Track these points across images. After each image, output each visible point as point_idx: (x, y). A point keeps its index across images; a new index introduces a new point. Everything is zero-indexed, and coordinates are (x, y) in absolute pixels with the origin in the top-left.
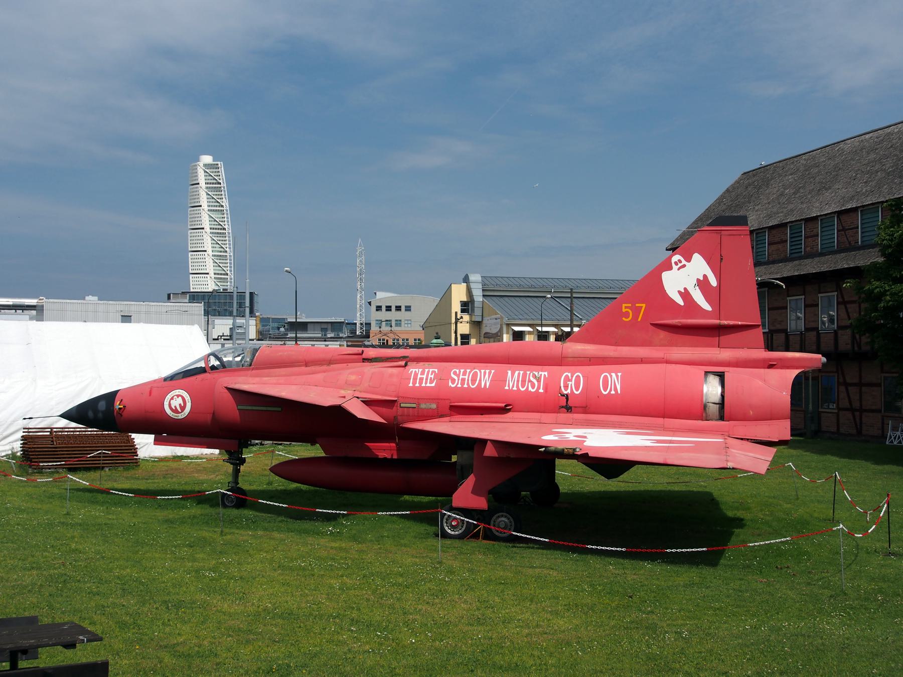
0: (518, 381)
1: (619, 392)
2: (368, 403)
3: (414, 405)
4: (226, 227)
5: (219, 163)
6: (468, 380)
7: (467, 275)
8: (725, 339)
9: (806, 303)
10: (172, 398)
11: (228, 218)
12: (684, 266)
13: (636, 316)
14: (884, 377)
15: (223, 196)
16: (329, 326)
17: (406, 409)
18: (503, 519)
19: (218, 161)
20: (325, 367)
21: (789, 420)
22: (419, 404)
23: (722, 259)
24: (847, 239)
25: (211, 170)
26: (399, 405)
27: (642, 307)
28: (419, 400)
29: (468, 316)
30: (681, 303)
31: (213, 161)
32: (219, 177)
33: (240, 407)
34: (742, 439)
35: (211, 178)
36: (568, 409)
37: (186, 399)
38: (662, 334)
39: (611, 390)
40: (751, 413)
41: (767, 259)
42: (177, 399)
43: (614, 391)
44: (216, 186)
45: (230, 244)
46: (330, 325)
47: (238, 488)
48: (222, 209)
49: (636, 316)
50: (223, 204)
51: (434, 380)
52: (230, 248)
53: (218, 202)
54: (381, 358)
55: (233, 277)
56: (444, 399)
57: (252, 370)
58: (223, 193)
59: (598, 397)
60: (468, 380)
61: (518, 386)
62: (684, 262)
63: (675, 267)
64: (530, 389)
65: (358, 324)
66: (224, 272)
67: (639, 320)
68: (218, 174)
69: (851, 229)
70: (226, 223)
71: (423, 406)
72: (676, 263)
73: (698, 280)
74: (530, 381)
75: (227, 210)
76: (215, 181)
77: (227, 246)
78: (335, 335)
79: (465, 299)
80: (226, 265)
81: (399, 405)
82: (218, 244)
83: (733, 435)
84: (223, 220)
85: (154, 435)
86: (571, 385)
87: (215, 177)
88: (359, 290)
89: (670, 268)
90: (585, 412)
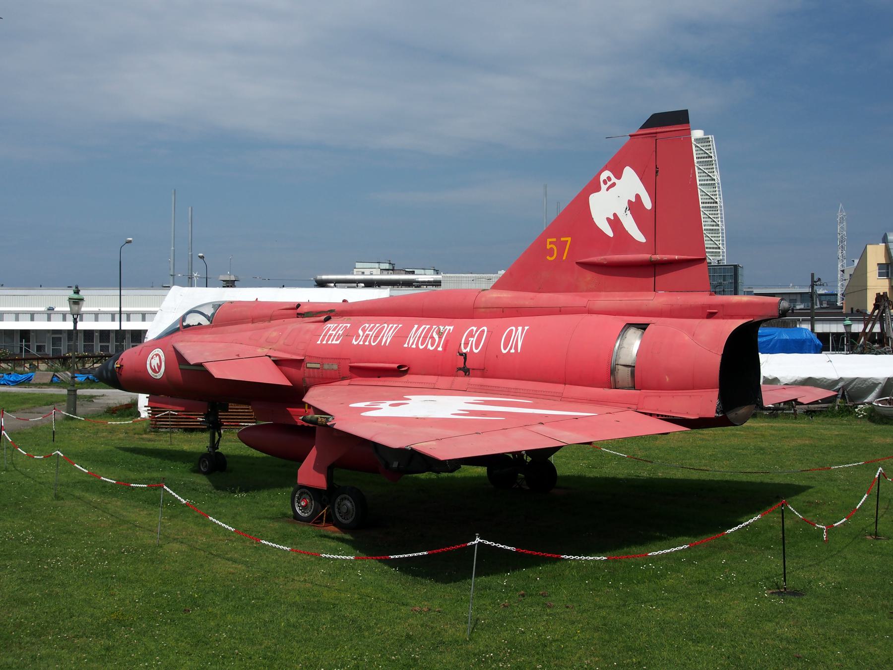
0: (419, 337)
1: (519, 351)
2: (278, 362)
3: (318, 366)
4: (717, 200)
5: (710, 136)
6: (372, 336)
7: (886, 234)
8: (664, 279)
10: (152, 358)
11: (719, 191)
12: (614, 185)
13: (560, 254)
15: (714, 170)
16: (799, 297)
17: (311, 369)
18: (349, 504)
19: (708, 135)
21: (718, 389)
22: (322, 365)
23: (657, 172)
25: (703, 144)
26: (305, 366)
27: (568, 241)
28: (322, 359)
29: (887, 280)
30: (609, 232)
31: (704, 135)
32: (710, 151)
33: (182, 367)
34: (651, 415)
35: (702, 152)
36: (466, 371)
37: (162, 358)
38: (589, 276)
39: (511, 349)
40: (668, 379)
43: (514, 349)
44: (708, 159)
45: (722, 218)
46: (799, 296)
47: (218, 452)
48: (714, 182)
49: (560, 254)
50: (715, 178)
51: (341, 336)
52: (722, 221)
53: (709, 176)
54: (312, 312)
55: (725, 250)
56: (345, 359)
57: (212, 327)
58: (714, 166)
59: (497, 356)
60: (372, 336)
61: (417, 344)
62: (614, 180)
63: (604, 187)
64: (429, 347)
65: (839, 295)
66: (716, 246)
67: (564, 258)
68: (709, 147)
70: (717, 196)
71: (326, 367)
72: (605, 182)
73: (630, 202)
74: (432, 337)
75: (718, 184)
76: (706, 155)
77: (719, 219)
78: (805, 306)
79: (883, 261)
80: (718, 239)
81: (305, 366)
82: (710, 218)
83: (642, 409)
84: (715, 193)
86: (473, 341)
87: (706, 151)
88: (841, 258)
89: (598, 189)
90: (483, 376)
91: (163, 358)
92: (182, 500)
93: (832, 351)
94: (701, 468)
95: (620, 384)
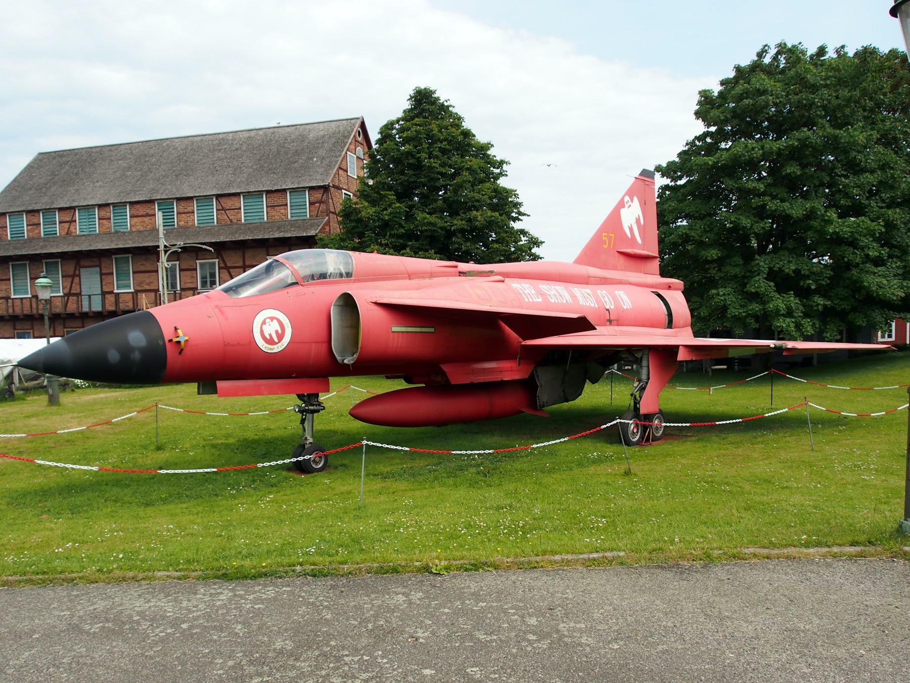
9: (181, 268)
10: (264, 323)
13: (610, 244)
14: (67, 331)
20: (427, 281)
24: (228, 217)
37: (284, 323)
38: (622, 260)
41: (129, 229)
42: (271, 323)
54: (474, 271)
62: (630, 203)
63: (627, 206)
69: (233, 209)
85: (197, 384)
89: (624, 206)
92: (93, 468)
94: (186, 211)
95: (118, 314)
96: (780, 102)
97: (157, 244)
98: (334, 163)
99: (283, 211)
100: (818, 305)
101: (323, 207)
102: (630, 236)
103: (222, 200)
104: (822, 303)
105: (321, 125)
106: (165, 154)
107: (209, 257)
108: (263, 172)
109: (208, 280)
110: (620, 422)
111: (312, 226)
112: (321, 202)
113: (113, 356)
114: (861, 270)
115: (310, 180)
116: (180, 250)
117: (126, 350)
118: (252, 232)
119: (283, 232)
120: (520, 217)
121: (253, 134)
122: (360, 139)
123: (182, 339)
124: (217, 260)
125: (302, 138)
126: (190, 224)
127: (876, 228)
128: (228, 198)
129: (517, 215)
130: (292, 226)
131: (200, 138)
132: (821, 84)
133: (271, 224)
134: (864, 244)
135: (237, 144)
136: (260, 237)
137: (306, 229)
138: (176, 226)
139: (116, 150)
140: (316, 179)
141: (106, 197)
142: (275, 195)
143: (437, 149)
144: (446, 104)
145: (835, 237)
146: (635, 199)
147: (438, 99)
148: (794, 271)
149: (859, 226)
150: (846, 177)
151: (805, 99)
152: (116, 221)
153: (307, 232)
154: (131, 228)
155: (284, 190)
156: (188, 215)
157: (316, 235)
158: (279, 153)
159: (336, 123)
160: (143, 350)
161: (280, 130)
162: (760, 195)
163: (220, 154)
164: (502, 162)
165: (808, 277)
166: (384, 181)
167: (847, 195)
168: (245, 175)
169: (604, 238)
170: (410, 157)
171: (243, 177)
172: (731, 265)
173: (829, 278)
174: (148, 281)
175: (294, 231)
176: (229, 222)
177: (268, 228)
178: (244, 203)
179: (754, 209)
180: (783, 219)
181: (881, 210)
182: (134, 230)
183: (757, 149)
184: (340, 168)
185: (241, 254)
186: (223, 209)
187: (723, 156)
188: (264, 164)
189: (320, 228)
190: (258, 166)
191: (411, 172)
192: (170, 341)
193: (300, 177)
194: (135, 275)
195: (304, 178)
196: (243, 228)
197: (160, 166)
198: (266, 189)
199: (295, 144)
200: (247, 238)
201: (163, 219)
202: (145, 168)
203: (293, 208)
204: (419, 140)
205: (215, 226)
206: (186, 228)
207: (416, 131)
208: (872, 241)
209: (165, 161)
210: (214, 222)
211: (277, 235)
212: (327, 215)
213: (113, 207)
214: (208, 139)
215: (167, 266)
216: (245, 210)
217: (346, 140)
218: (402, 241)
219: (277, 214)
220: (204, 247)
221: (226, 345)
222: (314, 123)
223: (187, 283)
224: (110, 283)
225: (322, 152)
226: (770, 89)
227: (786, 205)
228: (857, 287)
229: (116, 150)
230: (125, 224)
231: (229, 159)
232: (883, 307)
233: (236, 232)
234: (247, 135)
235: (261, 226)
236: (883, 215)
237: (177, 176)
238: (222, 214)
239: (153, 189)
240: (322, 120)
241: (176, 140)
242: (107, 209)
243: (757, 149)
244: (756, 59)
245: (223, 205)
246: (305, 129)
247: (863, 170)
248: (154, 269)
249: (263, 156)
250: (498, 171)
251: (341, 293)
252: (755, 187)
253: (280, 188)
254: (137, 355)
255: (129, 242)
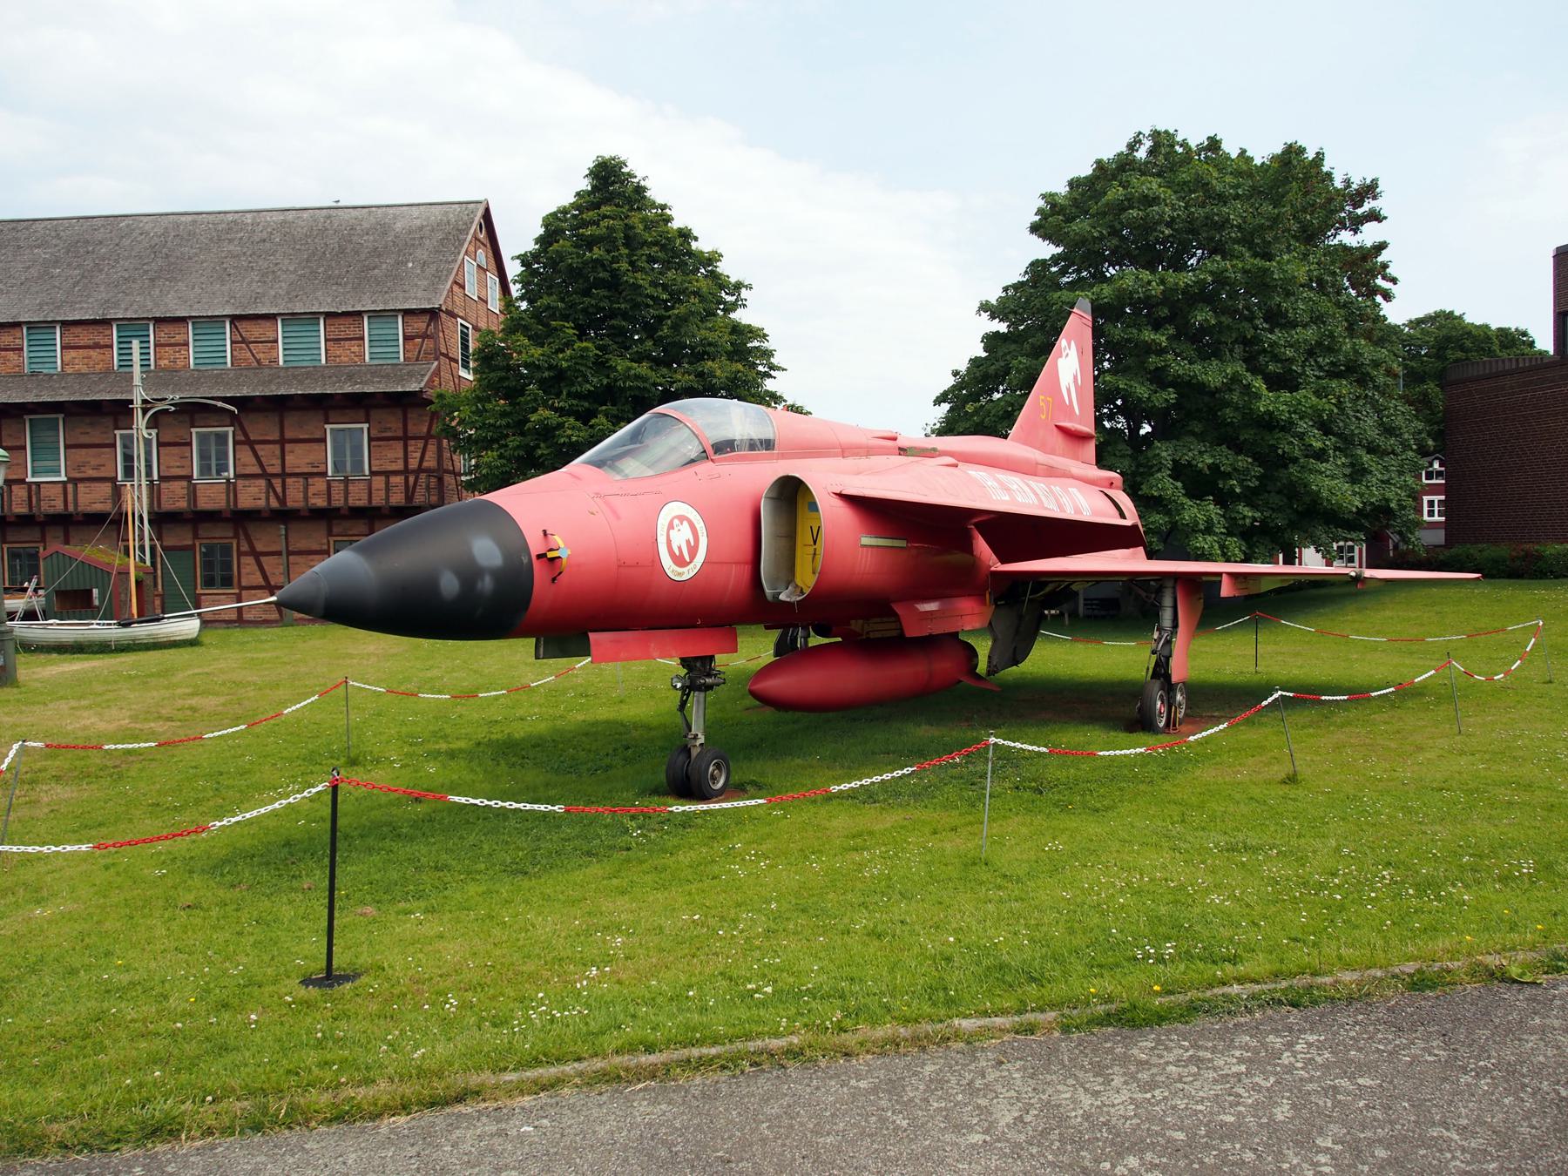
9: (161, 440)
10: (671, 526)
24: (253, 355)
37: (698, 526)
38: (1058, 440)
41: (59, 369)
63: (1064, 354)
69: (261, 342)
85: (534, 640)
89: (1061, 357)
91: (700, 526)
93: (1285, 563)
94: (173, 341)
96: (1178, 215)
97: (124, 397)
98: (445, 273)
99: (355, 349)
100: (1245, 517)
101: (428, 344)
102: (1067, 403)
103: (242, 326)
104: (1250, 514)
105: (414, 208)
106: (126, 242)
107: (216, 424)
108: (317, 282)
109: (213, 463)
110: (1282, 695)
111: (411, 374)
112: (424, 336)
113: (449, 585)
114: (1302, 467)
115: (406, 299)
116: (173, 408)
117: (469, 573)
118: (301, 383)
119: (359, 383)
120: (772, 372)
121: (290, 216)
122: (482, 236)
123: (564, 553)
124: (231, 429)
125: (383, 228)
126: (180, 364)
127: (1327, 407)
128: (254, 322)
129: (766, 369)
130: (374, 374)
131: (190, 218)
132: (1230, 194)
133: (335, 369)
134: (1302, 430)
135: (262, 231)
136: (318, 391)
137: (401, 380)
138: (152, 367)
139: (27, 229)
140: (416, 298)
141: (15, 311)
142: (341, 321)
143: (644, 258)
144: (642, 183)
145: (1267, 417)
146: (1073, 343)
147: (631, 175)
148: (1209, 467)
149: (1300, 403)
150: (1272, 332)
151: (1217, 215)
152: (32, 355)
153: (403, 386)
154: (62, 368)
155: (359, 314)
156: (177, 349)
157: (421, 392)
158: (342, 251)
159: (440, 207)
160: (497, 574)
161: (340, 212)
162: (1161, 352)
163: (231, 247)
164: (738, 286)
165: (1228, 476)
166: (555, 304)
167: (1276, 358)
168: (283, 284)
169: (1042, 404)
170: (600, 269)
171: (281, 288)
172: (1115, 455)
173: (1257, 478)
174: (94, 462)
175: (380, 382)
176: (255, 364)
177: (330, 377)
178: (283, 332)
179: (1150, 372)
180: (1189, 388)
181: (1320, 381)
182: (70, 371)
183: (1154, 283)
184: (456, 282)
185: (277, 419)
186: (244, 341)
187: (1104, 291)
188: (317, 268)
189: (426, 379)
190: (307, 270)
191: (603, 292)
192: (539, 557)
193: (386, 292)
194: (68, 450)
195: (394, 295)
196: (282, 374)
197: (117, 261)
198: (326, 310)
199: (371, 238)
200: (293, 391)
201: (141, 354)
202: (89, 263)
203: (374, 344)
204: (614, 242)
205: (229, 370)
206: (172, 371)
207: (608, 228)
208: (1312, 426)
209: (126, 254)
210: (226, 363)
211: (348, 389)
212: (437, 359)
213: (28, 328)
214: (206, 220)
215: (146, 436)
216: (284, 343)
217: (461, 237)
218: (586, 404)
219: (345, 353)
220: (220, 404)
221: (621, 565)
222: (423, 205)
223: (173, 467)
224: (18, 464)
225: (421, 254)
226: (1162, 196)
227: (1197, 367)
228: (1293, 491)
229: (27, 229)
230: (53, 360)
231: (251, 256)
232: (1327, 523)
233: (270, 382)
234: (281, 217)
235: (315, 372)
236: (1324, 388)
237: (152, 280)
238: (241, 349)
239: (107, 301)
240: (318, 205)
241: (145, 219)
242: (16, 332)
243: (1154, 283)
244: (1124, 149)
245: (243, 334)
246: (386, 215)
247: (1293, 325)
248: (18, 444)
249: (314, 254)
250: (733, 299)
251: (776, 478)
252: (1153, 340)
253: (351, 309)
254: (487, 584)
255: (62, 391)
